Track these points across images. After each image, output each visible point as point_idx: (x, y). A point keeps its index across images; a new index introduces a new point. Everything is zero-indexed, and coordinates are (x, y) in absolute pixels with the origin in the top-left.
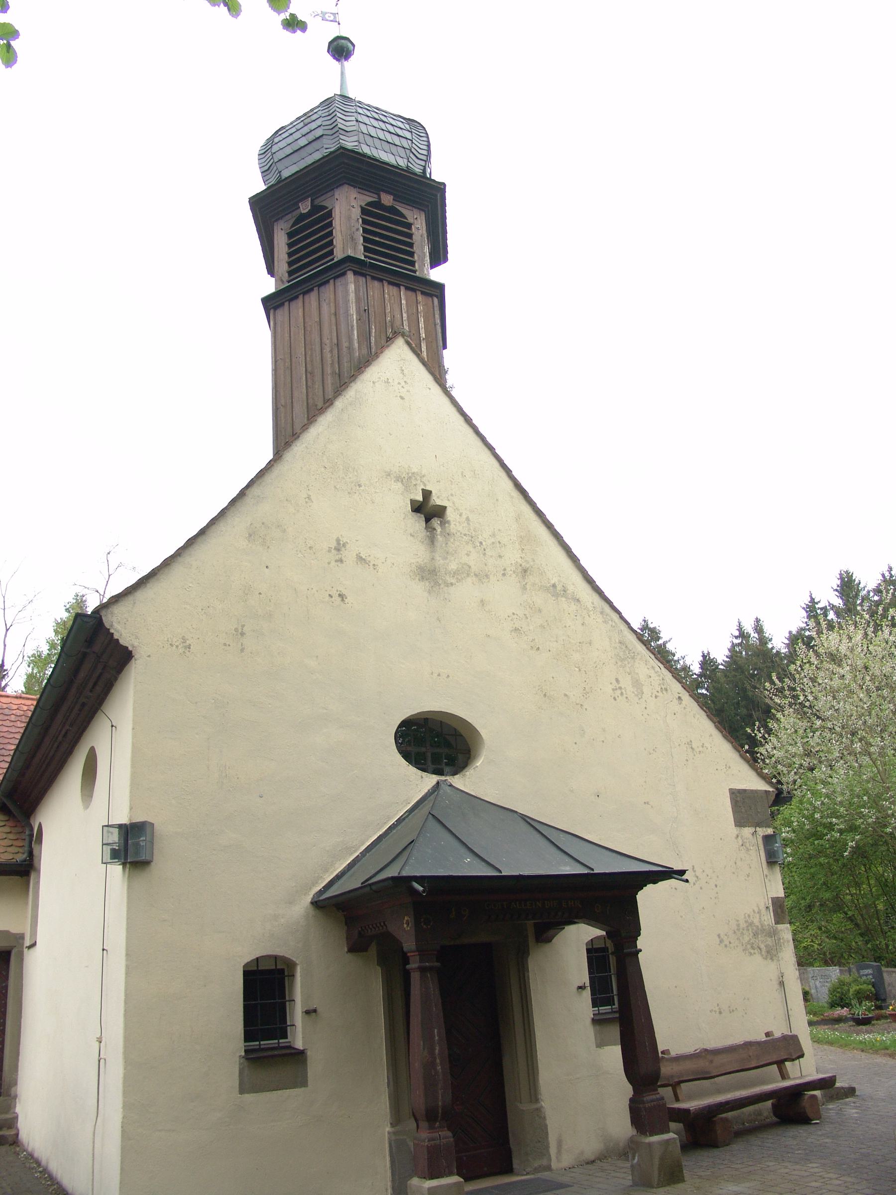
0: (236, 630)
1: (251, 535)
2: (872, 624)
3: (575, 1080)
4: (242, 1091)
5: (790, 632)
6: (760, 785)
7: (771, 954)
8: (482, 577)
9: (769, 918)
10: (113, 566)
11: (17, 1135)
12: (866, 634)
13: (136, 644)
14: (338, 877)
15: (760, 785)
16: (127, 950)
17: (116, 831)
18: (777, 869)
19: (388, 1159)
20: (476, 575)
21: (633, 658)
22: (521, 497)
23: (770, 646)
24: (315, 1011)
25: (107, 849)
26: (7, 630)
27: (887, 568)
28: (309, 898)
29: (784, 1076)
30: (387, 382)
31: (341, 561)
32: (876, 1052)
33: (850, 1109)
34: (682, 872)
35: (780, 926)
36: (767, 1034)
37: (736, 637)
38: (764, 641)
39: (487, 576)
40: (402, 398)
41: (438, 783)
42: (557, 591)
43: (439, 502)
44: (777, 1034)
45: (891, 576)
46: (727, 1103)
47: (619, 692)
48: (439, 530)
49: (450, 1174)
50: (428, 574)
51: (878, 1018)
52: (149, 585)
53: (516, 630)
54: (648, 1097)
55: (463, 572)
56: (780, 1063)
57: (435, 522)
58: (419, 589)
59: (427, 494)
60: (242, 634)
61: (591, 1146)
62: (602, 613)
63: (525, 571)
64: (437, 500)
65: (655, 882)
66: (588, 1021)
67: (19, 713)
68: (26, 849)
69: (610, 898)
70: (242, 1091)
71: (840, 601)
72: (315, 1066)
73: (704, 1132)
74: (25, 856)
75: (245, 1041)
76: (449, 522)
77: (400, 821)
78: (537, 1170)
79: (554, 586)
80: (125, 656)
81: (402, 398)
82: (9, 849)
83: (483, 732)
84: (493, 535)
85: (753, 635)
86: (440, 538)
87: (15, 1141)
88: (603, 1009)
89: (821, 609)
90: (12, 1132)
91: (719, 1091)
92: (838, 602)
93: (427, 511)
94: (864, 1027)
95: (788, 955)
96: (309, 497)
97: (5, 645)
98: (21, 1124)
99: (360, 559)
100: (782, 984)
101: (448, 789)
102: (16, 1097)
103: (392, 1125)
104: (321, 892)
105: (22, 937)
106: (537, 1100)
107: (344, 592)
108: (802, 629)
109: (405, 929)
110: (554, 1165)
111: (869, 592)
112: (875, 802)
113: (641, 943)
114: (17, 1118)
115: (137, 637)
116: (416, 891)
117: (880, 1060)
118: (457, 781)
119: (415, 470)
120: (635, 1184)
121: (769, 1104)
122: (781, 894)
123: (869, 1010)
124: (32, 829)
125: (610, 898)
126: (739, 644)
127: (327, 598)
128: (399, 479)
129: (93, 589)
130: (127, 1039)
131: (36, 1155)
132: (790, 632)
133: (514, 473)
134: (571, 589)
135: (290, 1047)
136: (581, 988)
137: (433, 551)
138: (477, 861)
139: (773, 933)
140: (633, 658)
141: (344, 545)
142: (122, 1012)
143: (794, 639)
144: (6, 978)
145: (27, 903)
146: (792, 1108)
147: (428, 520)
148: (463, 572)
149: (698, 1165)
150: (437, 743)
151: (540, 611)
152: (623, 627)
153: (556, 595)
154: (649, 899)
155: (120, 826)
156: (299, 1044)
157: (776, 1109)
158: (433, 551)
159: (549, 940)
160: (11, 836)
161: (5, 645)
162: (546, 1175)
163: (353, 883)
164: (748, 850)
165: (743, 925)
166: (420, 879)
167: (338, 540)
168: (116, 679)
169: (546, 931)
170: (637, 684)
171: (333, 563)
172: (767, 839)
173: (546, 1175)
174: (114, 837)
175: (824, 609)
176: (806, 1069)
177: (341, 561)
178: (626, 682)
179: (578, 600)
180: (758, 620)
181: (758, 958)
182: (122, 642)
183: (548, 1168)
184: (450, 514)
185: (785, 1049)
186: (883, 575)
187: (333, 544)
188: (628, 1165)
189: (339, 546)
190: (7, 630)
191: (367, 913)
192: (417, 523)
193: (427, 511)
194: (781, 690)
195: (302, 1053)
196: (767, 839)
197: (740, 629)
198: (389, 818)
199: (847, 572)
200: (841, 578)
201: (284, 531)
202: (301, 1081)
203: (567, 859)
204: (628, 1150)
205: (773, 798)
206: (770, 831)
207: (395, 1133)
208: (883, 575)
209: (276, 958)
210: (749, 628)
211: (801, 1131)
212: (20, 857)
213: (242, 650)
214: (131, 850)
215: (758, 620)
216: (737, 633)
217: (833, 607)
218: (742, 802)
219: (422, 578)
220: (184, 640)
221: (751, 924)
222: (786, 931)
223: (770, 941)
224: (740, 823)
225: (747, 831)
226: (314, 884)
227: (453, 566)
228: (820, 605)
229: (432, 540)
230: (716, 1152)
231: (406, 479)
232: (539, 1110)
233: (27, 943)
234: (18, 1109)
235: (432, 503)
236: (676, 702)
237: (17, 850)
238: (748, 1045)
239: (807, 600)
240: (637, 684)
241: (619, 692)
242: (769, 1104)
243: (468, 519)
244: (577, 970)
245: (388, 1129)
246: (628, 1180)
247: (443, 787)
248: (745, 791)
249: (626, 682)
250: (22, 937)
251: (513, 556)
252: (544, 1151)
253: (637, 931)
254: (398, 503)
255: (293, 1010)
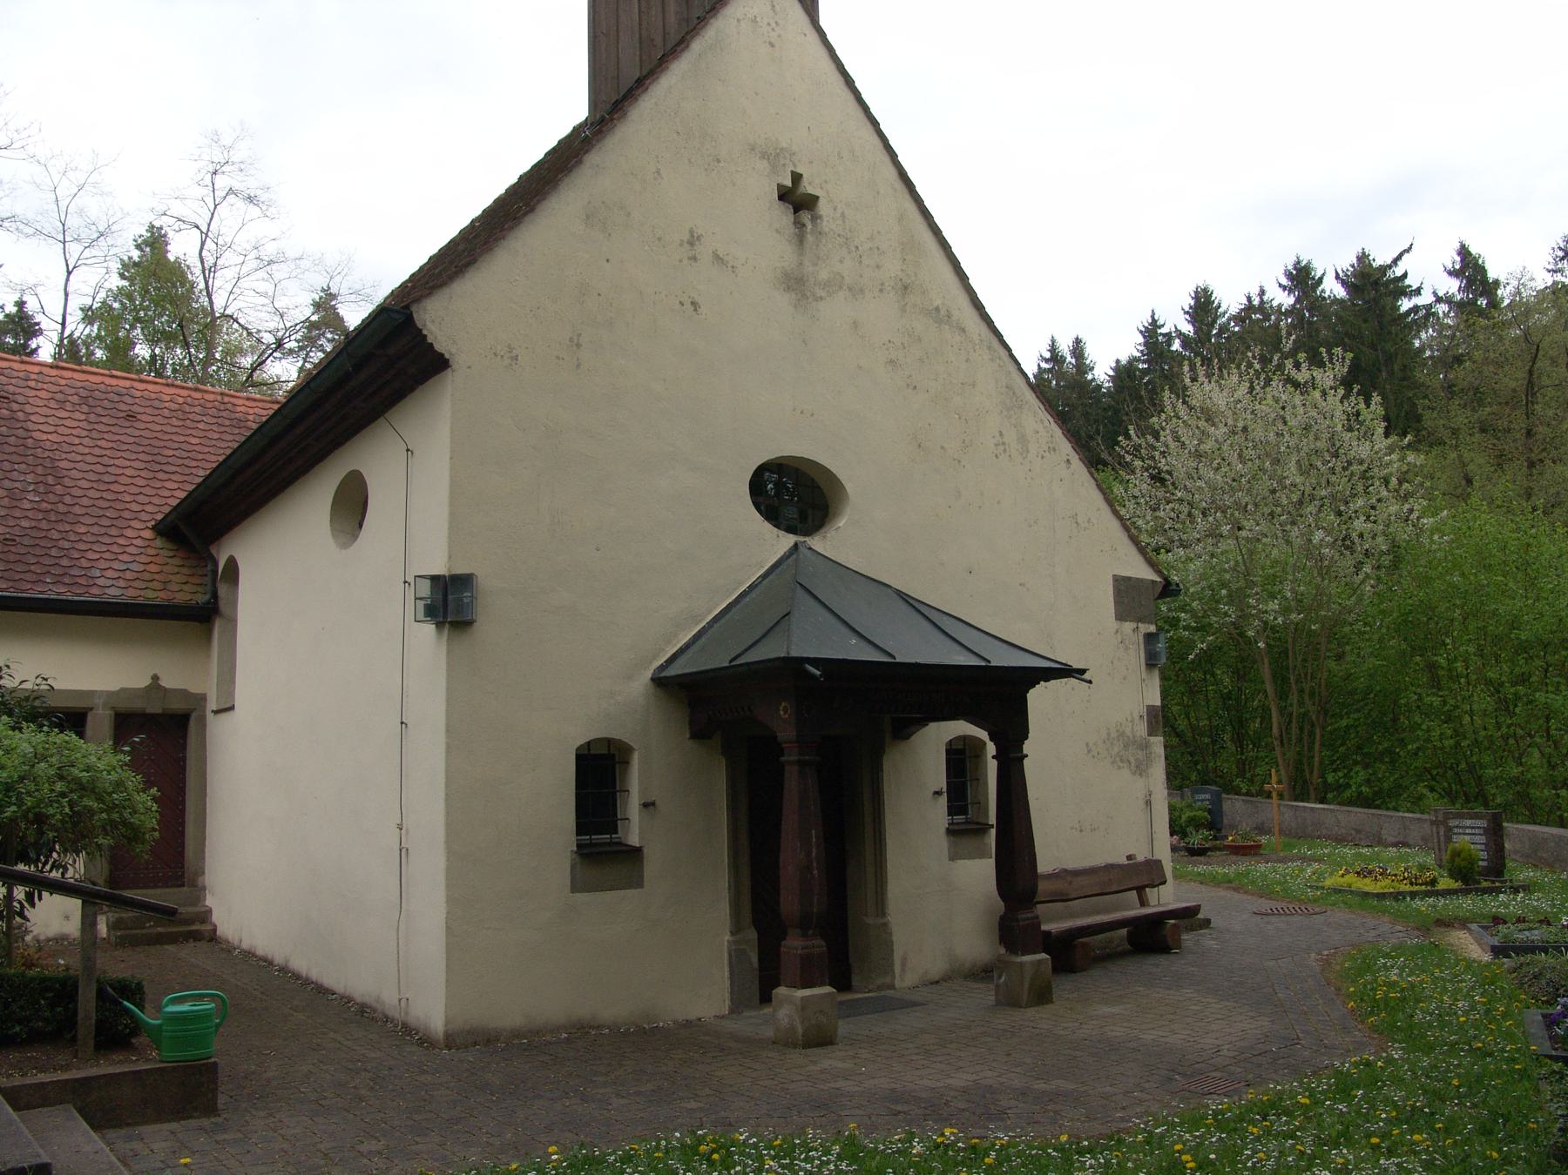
0: (571, 340)
1: (589, 218)
2: (1263, 376)
3: (934, 893)
4: (574, 889)
5: (1118, 361)
6: (1148, 574)
7: (1141, 769)
8: (856, 291)
9: (1141, 729)
10: (220, 194)
11: (215, 930)
12: (1252, 388)
13: (454, 351)
14: (682, 651)
15: (1148, 574)
16: (448, 725)
17: (428, 582)
18: (1156, 673)
19: (727, 969)
20: (850, 289)
21: (1020, 407)
22: (905, 191)
23: (1090, 377)
24: (653, 804)
25: (421, 604)
26: (69, 273)
27: (1257, 291)
28: (649, 674)
29: (1143, 902)
30: (754, 20)
31: (694, 259)
32: (1218, 885)
33: (1207, 940)
34: (1083, 671)
35: (1152, 739)
36: (1129, 857)
37: (1047, 361)
38: (1082, 366)
39: (862, 290)
40: (772, 45)
41: (796, 545)
42: (940, 316)
43: (810, 191)
44: (1140, 858)
45: (1262, 302)
46: (1089, 927)
47: (1001, 448)
48: (809, 227)
49: (822, 984)
50: (795, 284)
51: (1215, 849)
52: (468, 275)
53: (892, 361)
54: (1023, 915)
55: (834, 285)
56: (1140, 890)
57: (805, 216)
58: (783, 300)
59: (797, 178)
60: (578, 345)
61: (937, 967)
62: (989, 348)
63: (906, 288)
64: (808, 187)
65: (1047, 680)
66: (943, 831)
67: (173, 406)
68: (209, 588)
69: (996, 696)
70: (574, 889)
71: (1191, 328)
72: (651, 867)
73: (1069, 954)
74: (207, 597)
75: (579, 832)
76: (820, 217)
77: (752, 587)
78: (880, 988)
79: (937, 309)
80: (435, 364)
81: (772, 45)
82: (185, 587)
83: (849, 487)
84: (871, 238)
85: (1069, 359)
86: (810, 238)
87: (213, 937)
88: (960, 818)
89: (1164, 335)
90: (209, 927)
91: (1072, 916)
92: (1187, 329)
93: (797, 200)
94: (1202, 859)
95: (1158, 771)
96: (658, 172)
97: (66, 295)
98: (216, 917)
99: (718, 259)
100: (1148, 803)
101: (809, 553)
102: (204, 888)
103: (732, 934)
104: (662, 668)
105: (202, 698)
106: (884, 914)
107: (697, 299)
108: (1136, 359)
109: (782, 720)
110: (897, 984)
111: (1229, 319)
112: (1237, 598)
113: (1027, 747)
114: (210, 911)
115: (454, 342)
116: (813, 676)
117: (1222, 893)
118: (816, 542)
119: (784, 145)
120: (998, 1003)
121: (1124, 931)
122: (1158, 703)
123: (1206, 839)
124: (216, 564)
125: (996, 696)
126: (1049, 371)
127: (678, 306)
128: (764, 156)
129: (190, 223)
130: (448, 825)
131: (260, 952)
132: (1118, 361)
133: (900, 159)
134: (956, 314)
135: (620, 844)
136: (938, 793)
137: (801, 254)
138: (863, 644)
139: (1145, 746)
140: (1020, 407)
141: (699, 238)
142: (442, 795)
143: (1124, 373)
144: (184, 747)
145: (209, 657)
146: (1152, 936)
147: (796, 211)
148: (834, 285)
149: (1064, 987)
150: (794, 494)
151: (920, 340)
152: (1012, 368)
153: (939, 321)
154: (1039, 698)
155: (434, 579)
156: (634, 840)
157: (1131, 937)
158: (801, 254)
159: (908, 737)
160: (185, 571)
161: (66, 295)
162: (890, 993)
163: (719, 659)
164: (1127, 649)
165: (1114, 735)
166: (816, 662)
167: (691, 232)
168: (412, 389)
169: (904, 729)
170: (1022, 439)
171: (685, 262)
172: (1149, 638)
173: (890, 993)
174: (425, 589)
175: (1168, 335)
176: (1166, 897)
177: (694, 259)
178: (1011, 437)
179: (964, 330)
180: (1078, 341)
181: (1126, 773)
182: (437, 347)
183: (892, 987)
184: (823, 207)
185: (1146, 875)
186: (1249, 299)
187: (686, 237)
188: (992, 986)
189: (693, 240)
190: (69, 273)
191: (716, 699)
192: (783, 216)
193: (797, 200)
194: (1137, 448)
195: (639, 850)
196: (1149, 638)
197: (1053, 348)
198: (740, 584)
199: (1205, 290)
200: (1197, 297)
201: (629, 215)
202: (637, 882)
203: (958, 648)
204: (983, 973)
205: (1159, 589)
206: (1152, 628)
207: (735, 942)
208: (1249, 299)
209: (609, 741)
210: (1065, 347)
211: (1162, 960)
212: (201, 598)
213: (578, 366)
214: (451, 607)
215: (1078, 341)
216: (1048, 355)
217: (1180, 334)
218: (1125, 589)
219: (788, 289)
220: (511, 349)
221: (1122, 734)
222: (1158, 744)
223: (1141, 755)
224: (1121, 617)
225: (1128, 626)
226: (655, 658)
227: (824, 275)
228: (1164, 330)
229: (800, 239)
230: (1072, 977)
231: (773, 156)
232: (885, 925)
233: (212, 705)
234: (209, 901)
235: (801, 190)
236: (1064, 465)
237: (195, 589)
238: (1110, 867)
239: (1146, 320)
240: (1022, 439)
241: (1001, 448)
242: (1124, 931)
243: (843, 215)
244: (936, 775)
245: (727, 937)
246: (991, 999)
247: (802, 549)
248: (1130, 578)
249: (1011, 437)
250: (202, 698)
251: (892, 267)
252: (888, 968)
253: (1025, 734)
254: (762, 186)
255: (625, 804)
